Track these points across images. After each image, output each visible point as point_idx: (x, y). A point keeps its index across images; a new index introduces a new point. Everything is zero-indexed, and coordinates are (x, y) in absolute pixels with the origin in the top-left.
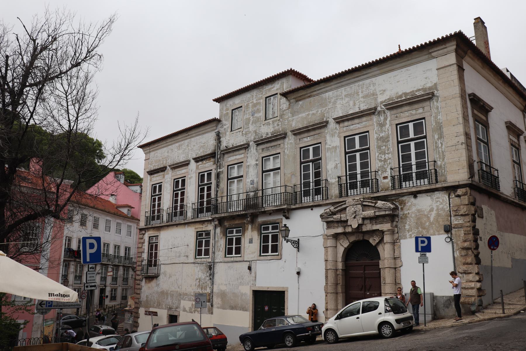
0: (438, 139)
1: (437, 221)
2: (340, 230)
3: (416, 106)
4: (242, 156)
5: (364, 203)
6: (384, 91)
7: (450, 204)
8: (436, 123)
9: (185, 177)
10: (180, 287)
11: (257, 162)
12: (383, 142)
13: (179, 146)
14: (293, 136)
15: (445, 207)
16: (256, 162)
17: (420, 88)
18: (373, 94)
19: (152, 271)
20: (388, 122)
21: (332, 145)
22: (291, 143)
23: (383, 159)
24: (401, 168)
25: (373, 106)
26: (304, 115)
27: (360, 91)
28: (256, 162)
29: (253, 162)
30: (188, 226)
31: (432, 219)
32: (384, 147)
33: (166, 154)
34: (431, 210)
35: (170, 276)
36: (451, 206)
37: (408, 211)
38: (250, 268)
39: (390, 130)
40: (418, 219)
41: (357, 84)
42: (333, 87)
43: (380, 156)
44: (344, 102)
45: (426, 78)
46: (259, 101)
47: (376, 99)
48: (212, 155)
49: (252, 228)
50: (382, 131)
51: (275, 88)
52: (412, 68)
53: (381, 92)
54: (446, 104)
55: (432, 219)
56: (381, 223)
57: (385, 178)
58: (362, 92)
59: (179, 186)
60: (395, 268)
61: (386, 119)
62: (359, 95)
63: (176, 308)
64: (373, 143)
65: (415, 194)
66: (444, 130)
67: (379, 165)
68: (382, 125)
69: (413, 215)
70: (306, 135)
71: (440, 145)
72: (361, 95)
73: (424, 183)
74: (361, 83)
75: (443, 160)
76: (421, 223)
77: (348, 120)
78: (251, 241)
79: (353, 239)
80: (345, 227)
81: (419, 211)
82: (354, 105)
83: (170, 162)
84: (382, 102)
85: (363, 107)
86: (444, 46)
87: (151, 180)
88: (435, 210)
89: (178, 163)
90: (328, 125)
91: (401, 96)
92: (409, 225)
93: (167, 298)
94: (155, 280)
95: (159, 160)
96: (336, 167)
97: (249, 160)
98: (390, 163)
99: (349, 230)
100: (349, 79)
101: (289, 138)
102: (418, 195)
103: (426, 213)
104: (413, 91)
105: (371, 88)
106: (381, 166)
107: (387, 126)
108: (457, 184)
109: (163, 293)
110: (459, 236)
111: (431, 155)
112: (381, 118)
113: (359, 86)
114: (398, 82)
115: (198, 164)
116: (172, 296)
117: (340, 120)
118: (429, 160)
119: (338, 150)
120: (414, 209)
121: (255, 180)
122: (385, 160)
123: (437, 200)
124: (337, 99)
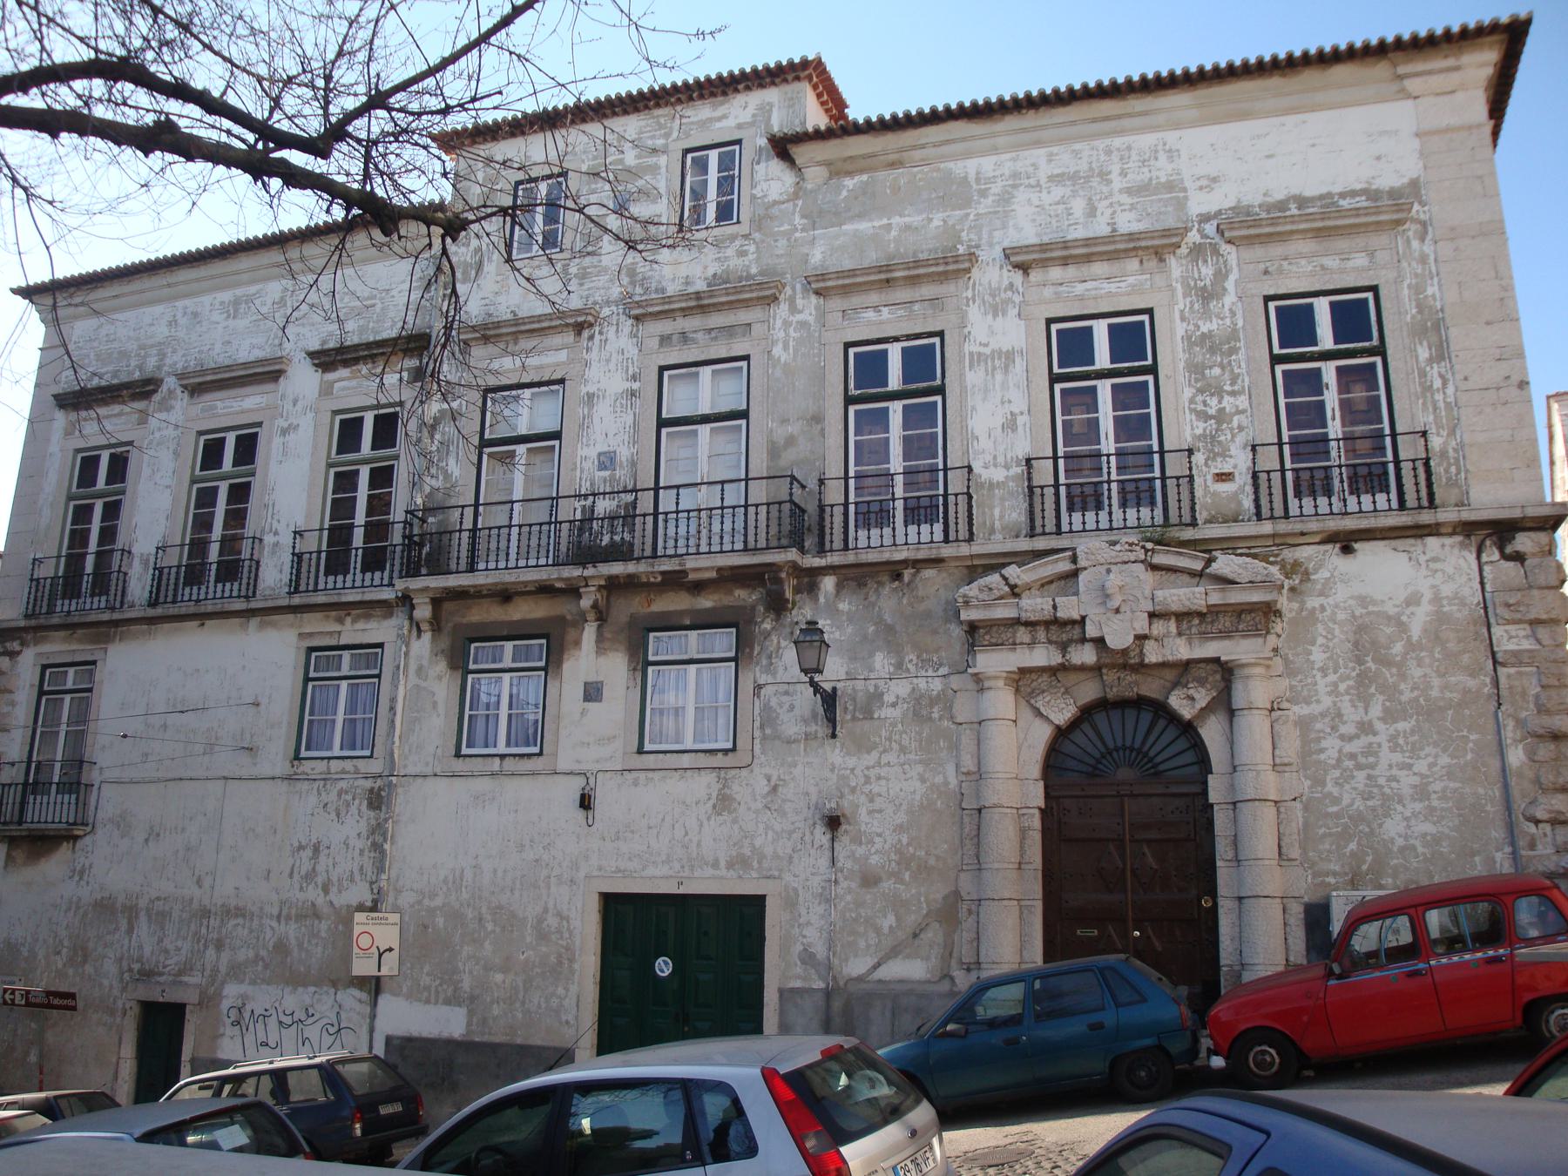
0: (1430, 361)
1: (1437, 637)
2: (1042, 656)
3: (1342, 244)
4: (563, 356)
5: (1159, 559)
6: (1215, 180)
7: (1482, 583)
8: (1420, 307)
9: (260, 424)
10: (207, 882)
11: (636, 386)
12: (1213, 350)
13: (236, 302)
14: (814, 299)
15: (1466, 591)
16: (628, 385)
17: (1358, 187)
18: (1170, 186)
19: (49, 811)
20: (1230, 284)
21: (994, 345)
22: (803, 325)
23: (1212, 412)
24: (1286, 449)
25: (1171, 222)
26: (863, 226)
27: (1115, 169)
28: (628, 385)
29: (616, 384)
30: (262, 626)
31: (1416, 631)
32: (1217, 371)
33: (162, 331)
34: (1413, 600)
35: (153, 835)
36: (1488, 588)
37: (1322, 600)
38: (585, 802)
39: (1241, 315)
40: (1361, 629)
41: (1100, 144)
42: (1001, 141)
43: (1199, 398)
44: (1047, 199)
45: (1378, 158)
46: (652, 160)
47: (1181, 204)
48: (414, 343)
49: (600, 639)
50: (1206, 314)
51: (730, 122)
52: (1317, 122)
53: (1204, 182)
54: (1456, 249)
55: (1416, 631)
56: (1226, 634)
57: (1223, 477)
58: (1123, 174)
59: (229, 460)
60: (1234, 803)
61: (1221, 276)
62: (1109, 182)
63: (181, 973)
64: (1172, 351)
65: (1346, 542)
66: (1454, 332)
67: (1199, 431)
68: (1207, 295)
69: (1341, 616)
70: (874, 298)
71: (1437, 383)
72: (1118, 183)
73: (1378, 508)
74: (1118, 142)
75: (1452, 432)
76: (1373, 643)
77: (1065, 262)
78: (593, 693)
79: (1089, 691)
80: (1064, 647)
81: (1363, 600)
82: (1092, 212)
83: (177, 360)
84: (1205, 218)
85: (1128, 223)
86: (1451, 62)
87: (68, 433)
88: (1425, 600)
89: (229, 368)
90: (975, 273)
91: (1282, 205)
92: (1326, 648)
93: (130, 931)
94: (64, 850)
95: (124, 354)
96: (1010, 425)
97: (594, 373)
98: (1241, 428)
99: (1085, 655)
100: (1073, 123)
101: (792, 301)
102: (1356, 546)
103: (1392, 611)
104: (1329, 195)
105: (1159, 164)
106: (1204, 436)
107: (1229, 299)
108: (1517, 514)
109: (105, 908)
110: (1524, 694)
111: (1410, 412)
112: (1204, 270)
113: (1108, 152)
114: (1268, 157)
115: (331, 376)
116: (160, 918)
117: (1022, 262)
118: (1399, 429)
119: (1019, 365)
120: (1341, 594)
121: (624, 453)
122: (1221, 417)
123: (1432, 565)
124: (1014, 186)
